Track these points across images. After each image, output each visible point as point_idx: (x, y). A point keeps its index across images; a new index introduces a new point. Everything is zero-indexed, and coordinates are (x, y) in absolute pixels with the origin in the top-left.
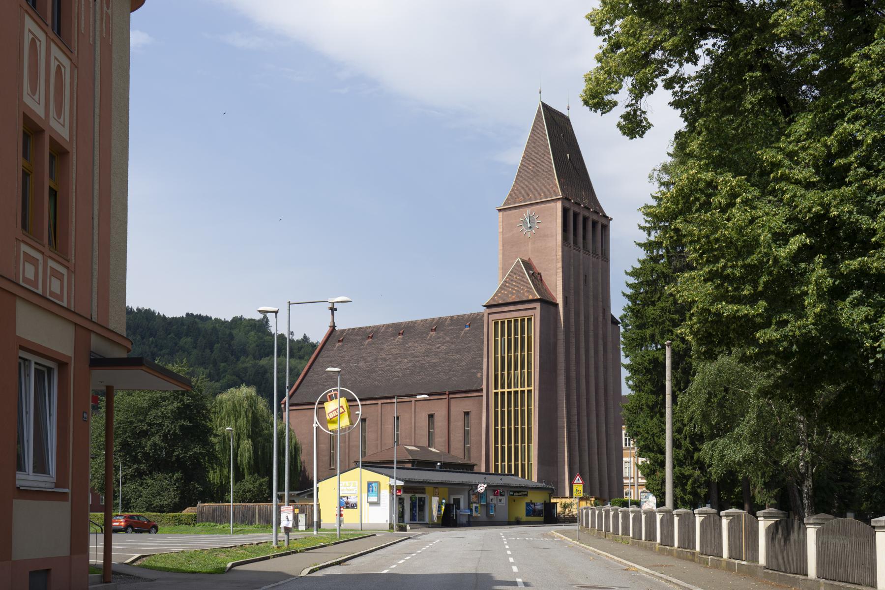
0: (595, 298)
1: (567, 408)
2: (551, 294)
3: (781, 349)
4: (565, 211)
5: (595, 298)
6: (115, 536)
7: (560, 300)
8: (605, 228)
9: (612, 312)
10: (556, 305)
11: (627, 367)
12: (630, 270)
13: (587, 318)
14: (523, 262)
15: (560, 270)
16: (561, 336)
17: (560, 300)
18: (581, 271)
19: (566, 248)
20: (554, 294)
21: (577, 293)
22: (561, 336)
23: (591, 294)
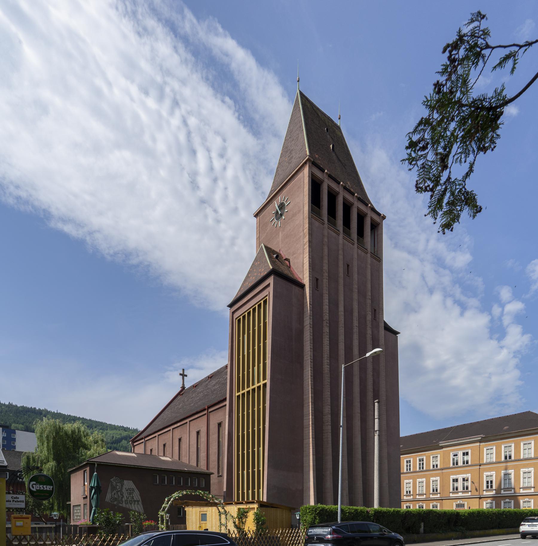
0: (362, 293)
1: (315, 403)
2: (296, 276)
3: (45, 513)
4: (315, 186)
5: (362, 293)
6: (408, 462)
7: (306, 280)
8: (376, 227)
9: (385, 319)
10: (302, 286)
11: (478, 137)
12: (440, 69)
13: (349, 312)
14: (266, 247)
15: (307, 246)
16: (308, 321)
17: (306, 280)
18: (341, 257)
19: (317, 224)
20: (301, 276)
21: (333, 278)
22: (308, 321)
23: (355, 286)
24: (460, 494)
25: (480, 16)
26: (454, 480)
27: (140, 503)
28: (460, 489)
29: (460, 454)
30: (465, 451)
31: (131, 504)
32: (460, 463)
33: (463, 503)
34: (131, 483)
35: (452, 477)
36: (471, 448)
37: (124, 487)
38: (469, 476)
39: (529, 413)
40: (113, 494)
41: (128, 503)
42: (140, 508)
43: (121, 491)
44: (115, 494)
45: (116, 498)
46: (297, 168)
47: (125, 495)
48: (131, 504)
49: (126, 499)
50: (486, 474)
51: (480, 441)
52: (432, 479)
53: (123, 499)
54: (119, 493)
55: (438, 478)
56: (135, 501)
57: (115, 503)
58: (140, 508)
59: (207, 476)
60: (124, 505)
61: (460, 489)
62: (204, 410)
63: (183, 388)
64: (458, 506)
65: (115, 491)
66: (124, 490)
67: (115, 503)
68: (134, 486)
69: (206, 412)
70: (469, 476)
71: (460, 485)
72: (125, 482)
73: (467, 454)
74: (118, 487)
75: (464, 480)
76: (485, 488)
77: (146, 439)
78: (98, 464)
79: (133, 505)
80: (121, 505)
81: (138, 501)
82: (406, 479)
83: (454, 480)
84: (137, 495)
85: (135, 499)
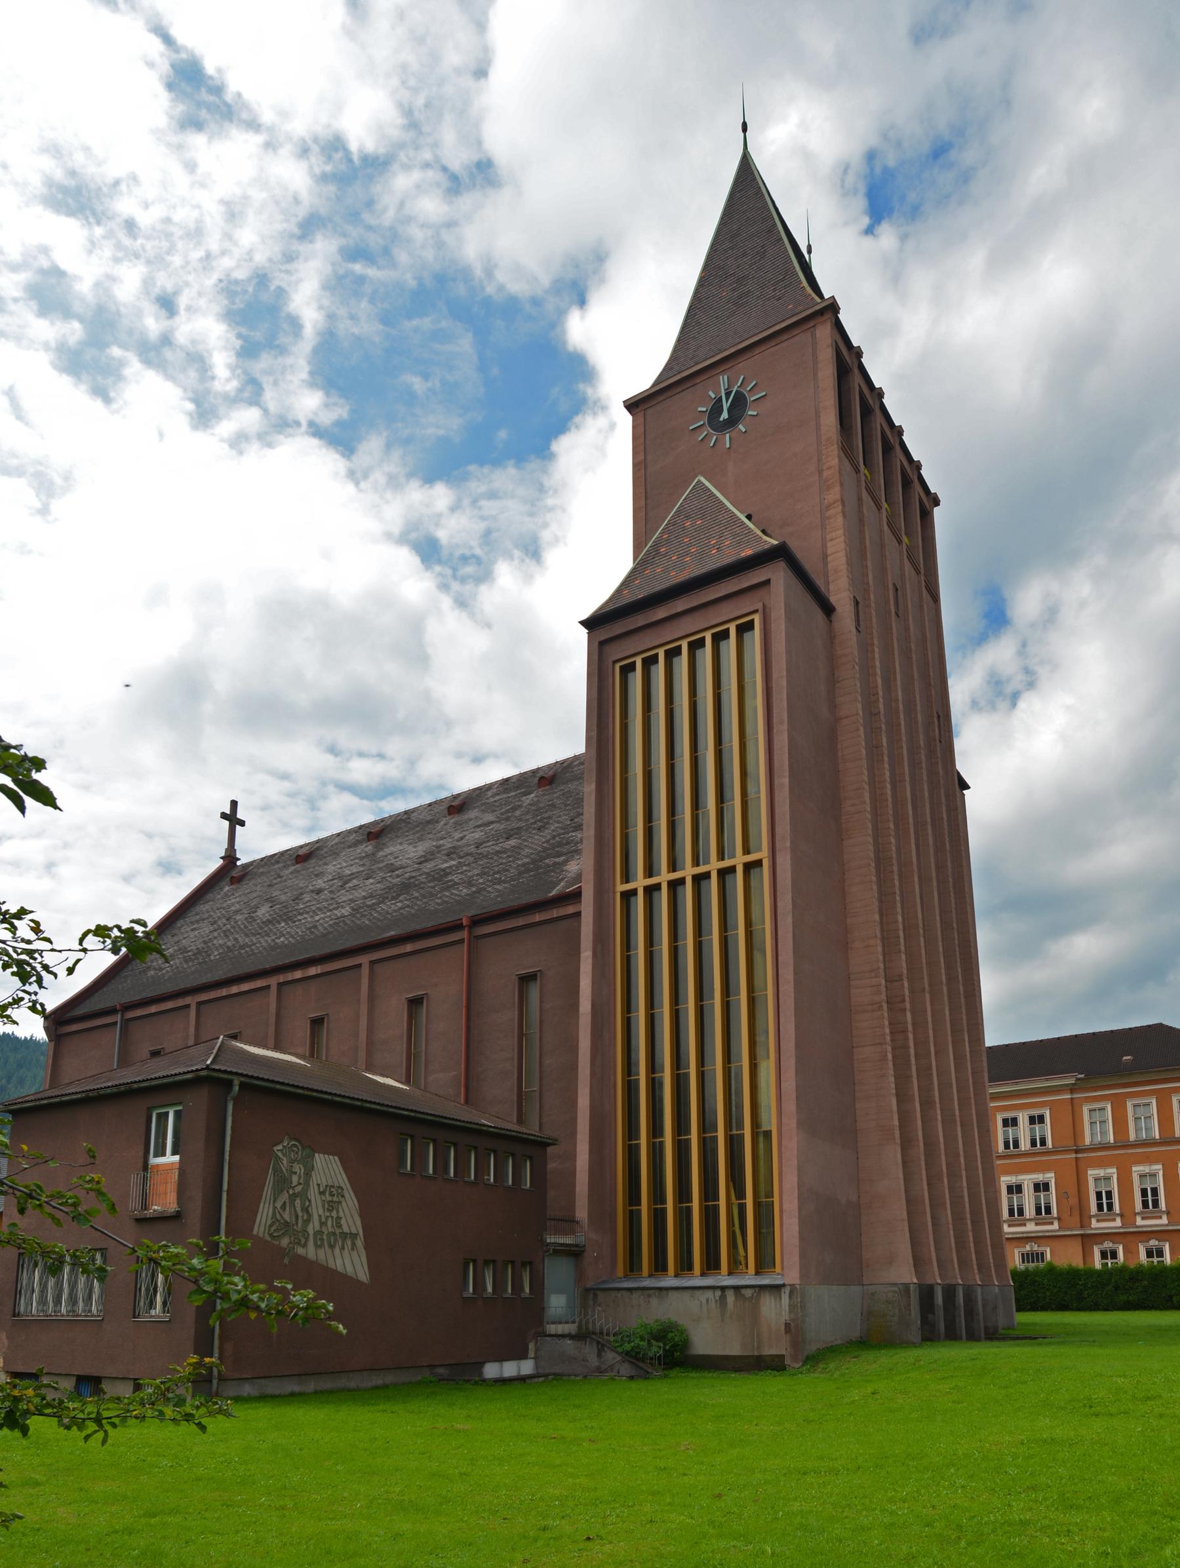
24: (1031, 1227)
25: (19, 207)
26: (1010, 1189)
27: (360, 1243)
28: (1029, 1211)
29: (1023, 1118)
30: (1036, 1112)
31: (332, 1247)
32: (1025, 1145)
33: (1042, 1249)
34: (335, 1161)
35: (1005, 1180)
36: (1051, 1105)
37: (315, 1179)
38: (1050, 1177)
39: (1161, 1025)
40: (278, 1205)
41: (322, 1246)
42: (358, 1266)
43: (303, 1195)
44: (284, 1207)
45: (287, 1224)
46: (733, 350)
47: (317, 1210)
48: (332, 1247)
49: (317, 1227)
50: (1092, 1173)
51: (1072, 1089)
52: (1137, 1169)
53: (311, 1230)
54: (298, 1202)
55: (1158, 1168)
56: (344, 1236)
57: (285, 1242)
58: (358, 1266)
59: (534, 1148)
60: (310, 1251)
61: (1029, 1211)
62: (457, 927)
63: (230, 857)
64: (1025, 1257)
65: (285, 1197)
66: (313, 1193)
67: (285, 1242)
68: (342, 1179)
69: (464, 934)
70: (1050, 1177)
71: (1028, 1200)
72: (319, 1158)
73: (1041, 1119)
74: (295, 1179)
75: (1037, 1187)
76: (1138, 1206)
77: (130, 1014)
78: (242, 1085)
79: (337, 1250)
80: (300, 1251)
81: (354, 1236)
82: (1007, 1173)
83: (1010, 1189)
84: (350, 1216)
85: (346, 1230)
